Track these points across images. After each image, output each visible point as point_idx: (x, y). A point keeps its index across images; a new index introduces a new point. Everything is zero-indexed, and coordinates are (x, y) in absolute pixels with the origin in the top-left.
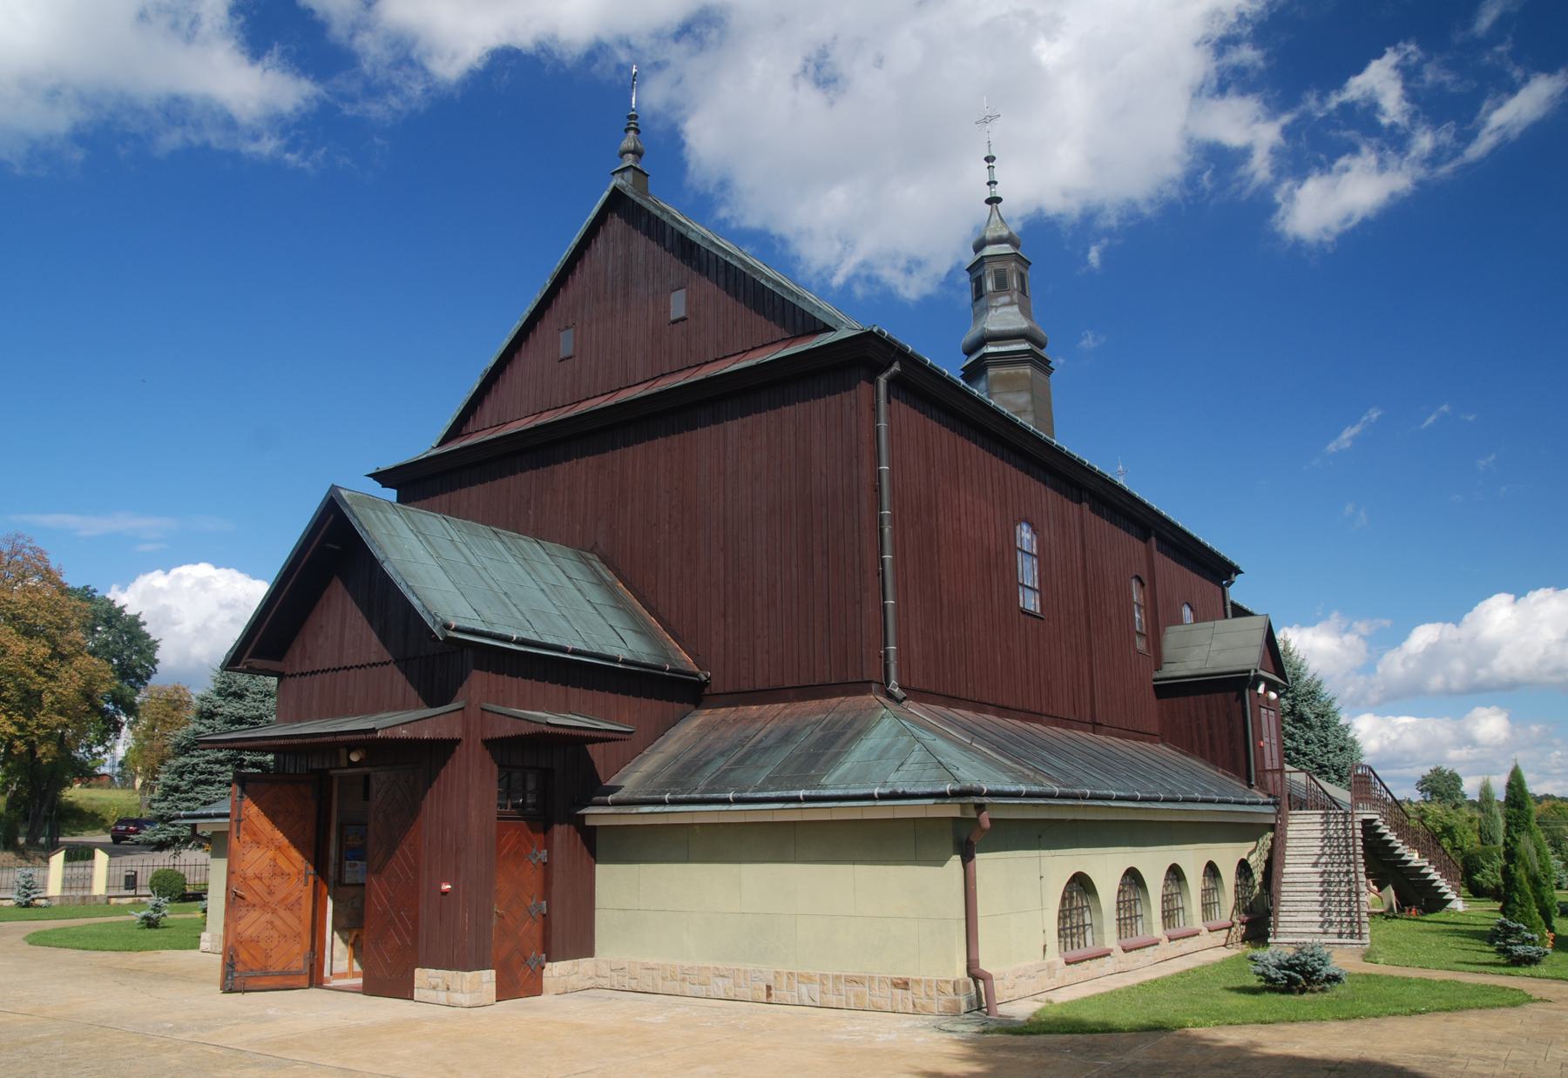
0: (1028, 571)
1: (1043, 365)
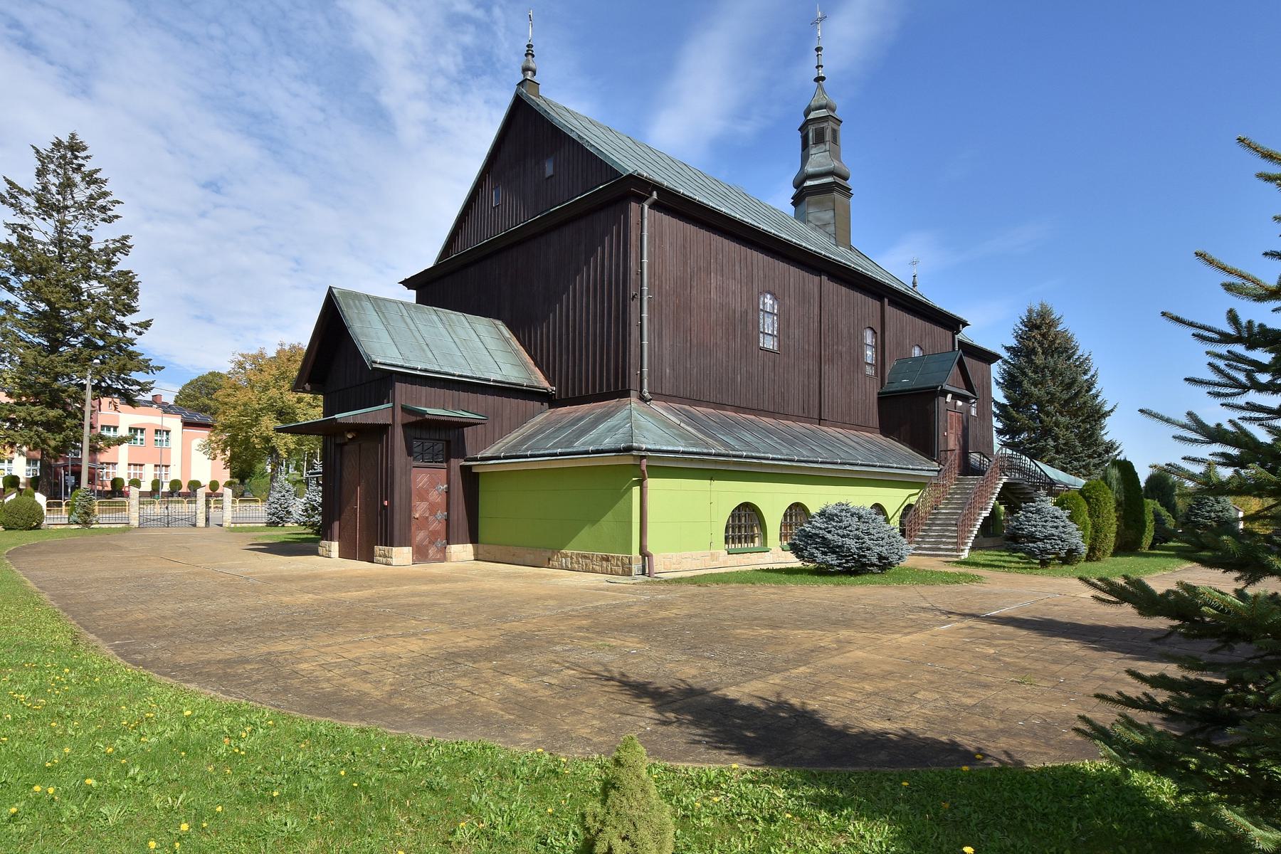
0: (769, 325)
1: (847, 191)
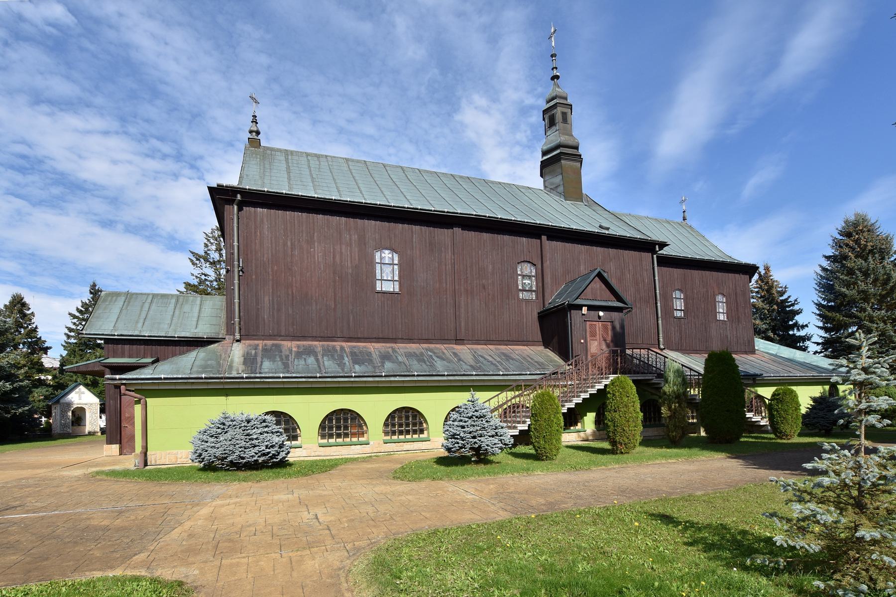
1: (578, 158)
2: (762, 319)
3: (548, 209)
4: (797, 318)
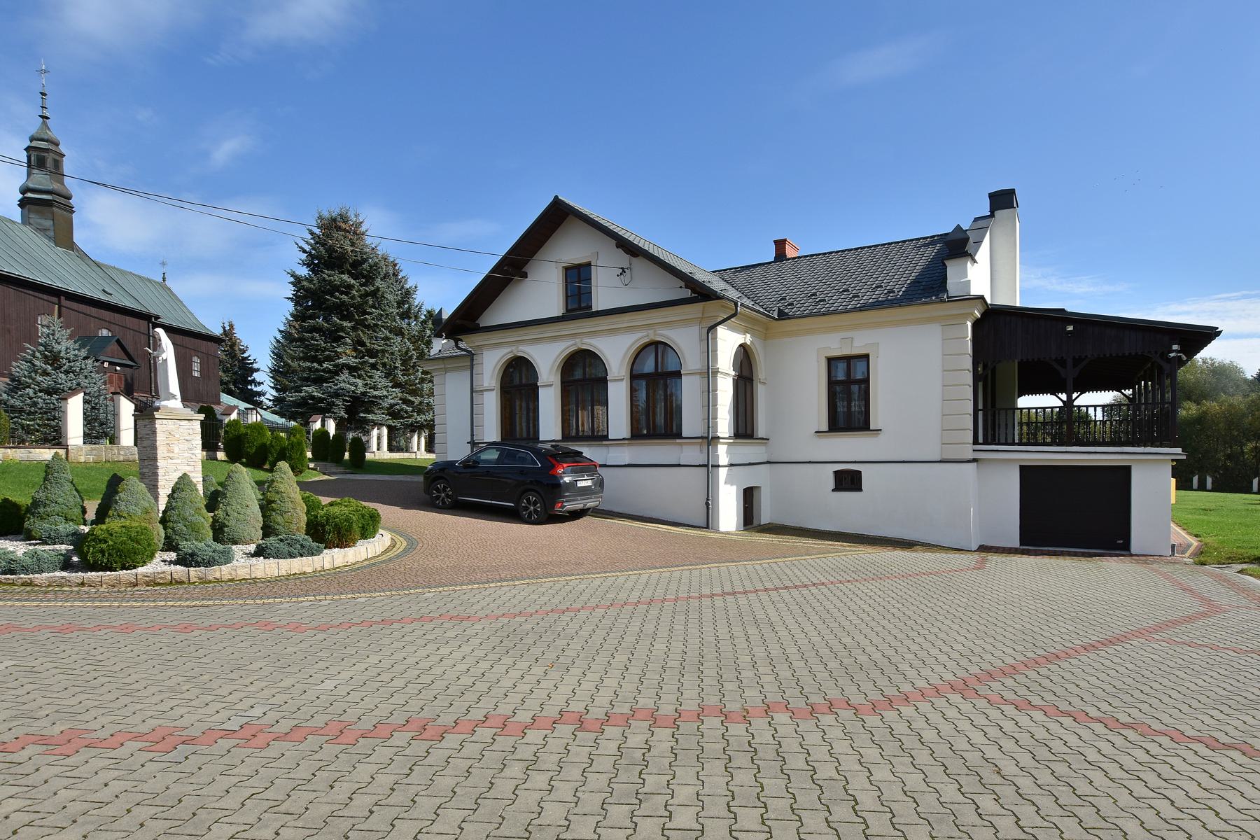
1: (70, 209)
2: (224, 372)
3: (48, 259)
4: (255, 375)
